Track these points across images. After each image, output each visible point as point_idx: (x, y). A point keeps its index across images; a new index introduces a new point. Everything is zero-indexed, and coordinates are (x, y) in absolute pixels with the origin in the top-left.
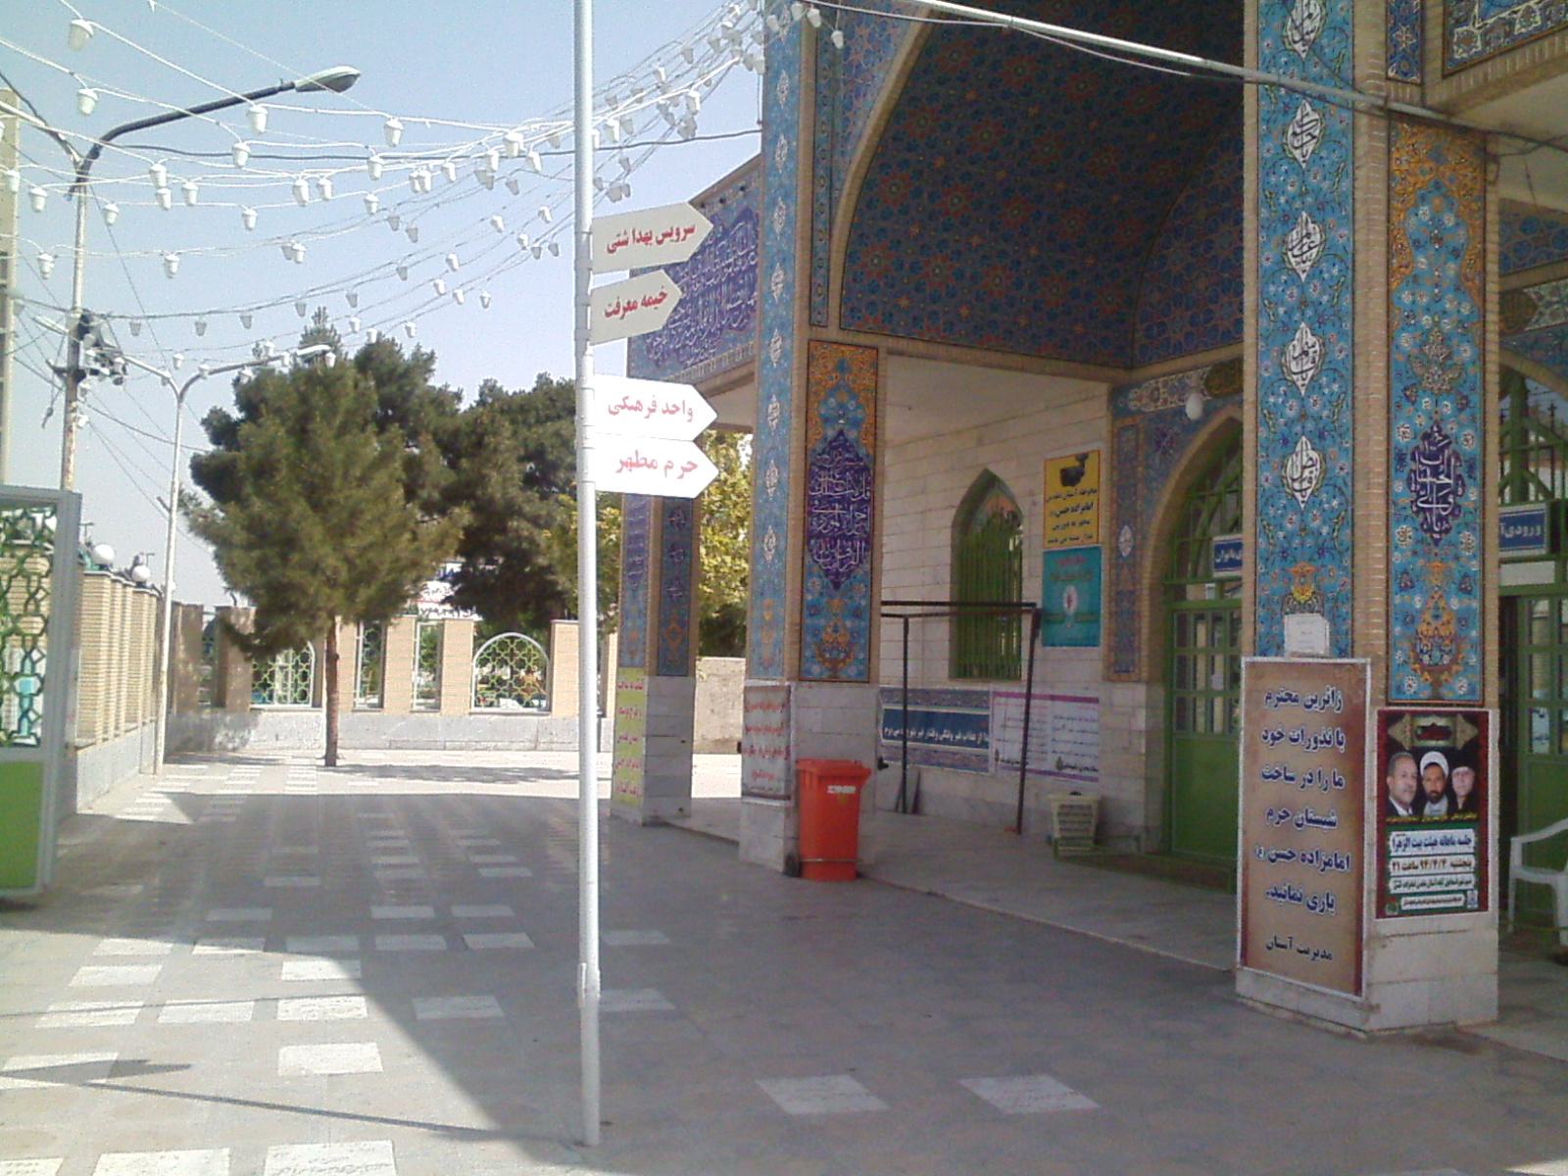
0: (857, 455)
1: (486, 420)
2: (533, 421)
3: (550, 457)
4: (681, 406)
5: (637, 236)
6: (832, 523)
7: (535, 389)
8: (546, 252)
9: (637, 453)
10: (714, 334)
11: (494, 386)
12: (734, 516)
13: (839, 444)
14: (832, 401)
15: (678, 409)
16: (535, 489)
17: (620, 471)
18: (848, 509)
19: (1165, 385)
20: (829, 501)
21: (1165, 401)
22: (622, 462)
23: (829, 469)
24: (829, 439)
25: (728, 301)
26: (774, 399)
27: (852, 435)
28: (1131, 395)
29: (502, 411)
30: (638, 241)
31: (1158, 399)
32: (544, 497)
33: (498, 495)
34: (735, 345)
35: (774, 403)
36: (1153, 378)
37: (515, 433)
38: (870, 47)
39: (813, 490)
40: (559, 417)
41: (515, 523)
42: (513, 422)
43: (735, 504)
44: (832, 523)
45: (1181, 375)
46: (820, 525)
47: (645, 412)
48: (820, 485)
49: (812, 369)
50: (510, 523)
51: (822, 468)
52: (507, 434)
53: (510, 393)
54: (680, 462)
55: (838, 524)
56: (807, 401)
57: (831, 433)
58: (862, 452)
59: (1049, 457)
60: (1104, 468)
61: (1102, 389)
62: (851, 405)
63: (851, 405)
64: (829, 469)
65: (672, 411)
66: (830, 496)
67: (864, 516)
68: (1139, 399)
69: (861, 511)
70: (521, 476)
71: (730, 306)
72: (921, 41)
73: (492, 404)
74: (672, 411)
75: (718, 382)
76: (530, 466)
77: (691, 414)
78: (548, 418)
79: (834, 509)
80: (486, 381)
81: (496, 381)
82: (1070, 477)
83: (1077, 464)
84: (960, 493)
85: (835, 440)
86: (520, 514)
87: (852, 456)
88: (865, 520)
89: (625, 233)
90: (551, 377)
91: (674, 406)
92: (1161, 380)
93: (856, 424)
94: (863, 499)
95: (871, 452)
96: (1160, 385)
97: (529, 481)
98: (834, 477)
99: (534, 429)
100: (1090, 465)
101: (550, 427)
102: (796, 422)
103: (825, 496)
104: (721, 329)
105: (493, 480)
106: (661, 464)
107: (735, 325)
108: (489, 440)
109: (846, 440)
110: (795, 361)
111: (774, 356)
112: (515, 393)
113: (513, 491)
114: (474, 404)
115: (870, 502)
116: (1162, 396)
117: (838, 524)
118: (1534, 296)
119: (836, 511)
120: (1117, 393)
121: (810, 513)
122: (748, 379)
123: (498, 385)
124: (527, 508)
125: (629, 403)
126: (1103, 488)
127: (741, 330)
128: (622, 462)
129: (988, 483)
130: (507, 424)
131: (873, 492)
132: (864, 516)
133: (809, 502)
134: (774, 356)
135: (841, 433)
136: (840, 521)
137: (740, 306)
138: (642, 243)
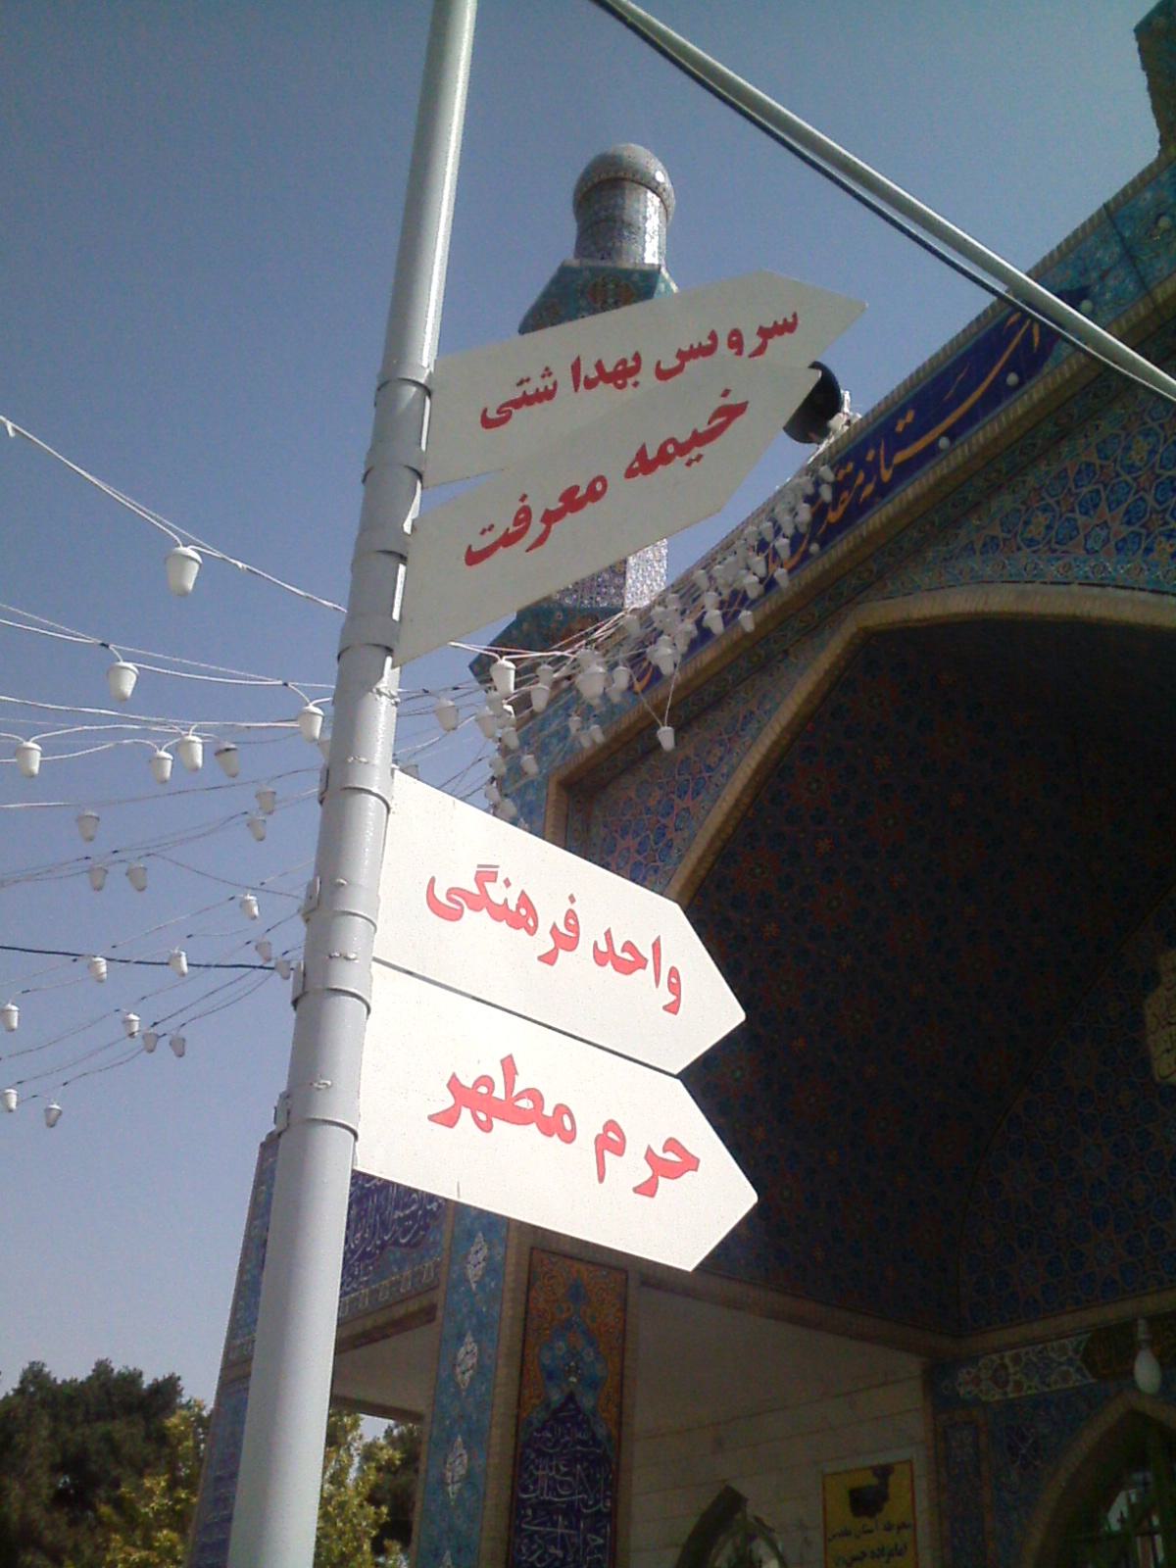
0: (594, 1436)
1: (21, 1414)
2: (79, 1418)
3: (94, 1468)
4: (647, 953)
5: (589, 371)
6: (552, 1550)
7: (90, 1378)
8: (163, 1045)
9: (608, 935)
10: (370, 1255)
11: (41, 1370)
12: (336, 1552)
13: (567, 1416)
14: (561, 1346)
15: (639, 963)
16: (66, 1509)
17: (448, 1119)
18: (577, 1528)
19: (1016, 1360)
20: (546, 1511)
21: (1018, 1385)
22: (454, 1084)
23: (551, 1457)
24: (554, 1406)
25: (396, 1207)
26: (469, 1338)
27: (587, 1402)
28: (963, 1375)
29: (44, 1403)
30: (590, 384)
31: (1007, 1383)
32: (73, 1523)
33: (15, 1517)
34: (400, 1269)
35: (470, 1344)
36: (996, 1351)
37: (53, 1435)
38: (639, 858)
39: (525, 1490)
40: (114, 1417)
41: (29, 1558)
42: (55, 1418)
43: (342, 1534)
44: (552, 1550)
45: (1040, 1346)
46: (532, 1553)
47: (544, 942)
48: (535, 1482)
49: (533, 1294)
50: (23, 1557)
51: (540, 1453)
52: (44, 1433)
53: (59, 1382)
54: (642, 1137)
55: (560, 1553)
56: (524, 1342)
57: (556, 1398)
58: (601, 1432)
59: (828, 1470)
60: (922, 1485)
61: (910, 1366)
62: (589, 1355)
63: (589, 1355)
64: (551, 1457)
65: (623, 960)
66: (550, 1502)
67: (600, 1541)
68: (977, 1381)
69: (597, 1532)
70: (52, 1492)
71: (399, 1214)
72: (719, 844)
73: (33, 1394)
74: (623, 960)
75: (369, 1323)
76: (64, 1480)
77: (675, 988)
78: (99, 1417)
79: (555, 1524)
80: (33, 1364)
81: (43, 1365)
82: (866, 1502)
83: (874, 1481)
84: (689, 1525)
85: (560, 1409)
86: (39, 1545)
87: (585, 1437)
88: (600, 1548)
89: (547, 373)
90: (113, 1365)
91: (629, 947)
92: (1008, 1354)
93: (594, 1385)
94: (599, 1512)
95: (614, 1432)
96: (1007, 1361)
97: (61, 1498)
98: (558, 1470)
99: (79, 1431)
100: (897, 1485)
101: (101, 1427)
102: (505, 1374)
103: (543, 1502)
104: (383, 1247)
105: (13, 1494)
106: (588, 1129)
107: (403, 1241)
108: (20, 1438)
109: (578, 1410)
110: (509, 1279)
111: (473, 1273)
112: (64, 1381)
113: (35, 1512)
114: (11, 1393)
115: (611, 1516)
116: (1011, 1378)
117: (560, 1553)
118: (1087, 1372)
119: (559, 1531)
120: (937, 1376)
121: (519, 1530)
122: (428, 1314)
123: (46, 1370)
124: (49, 1536)
125: (496, 893)
126: (922, 1519)
127: (416, 1245)
128: (454, 1084)
129: (729, 1504)
130: (46, 1420)
131: (615, 1501)
132: (600, 1541)
133: (516, 1507)
134: (473, 1273)
135: (570, 1398)
136: (564, 1548)
137: (414, 1213)
138: (604, 389)
